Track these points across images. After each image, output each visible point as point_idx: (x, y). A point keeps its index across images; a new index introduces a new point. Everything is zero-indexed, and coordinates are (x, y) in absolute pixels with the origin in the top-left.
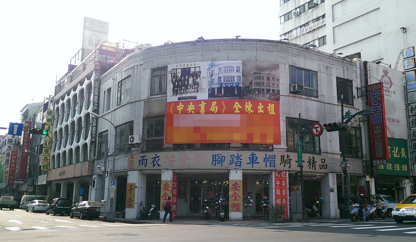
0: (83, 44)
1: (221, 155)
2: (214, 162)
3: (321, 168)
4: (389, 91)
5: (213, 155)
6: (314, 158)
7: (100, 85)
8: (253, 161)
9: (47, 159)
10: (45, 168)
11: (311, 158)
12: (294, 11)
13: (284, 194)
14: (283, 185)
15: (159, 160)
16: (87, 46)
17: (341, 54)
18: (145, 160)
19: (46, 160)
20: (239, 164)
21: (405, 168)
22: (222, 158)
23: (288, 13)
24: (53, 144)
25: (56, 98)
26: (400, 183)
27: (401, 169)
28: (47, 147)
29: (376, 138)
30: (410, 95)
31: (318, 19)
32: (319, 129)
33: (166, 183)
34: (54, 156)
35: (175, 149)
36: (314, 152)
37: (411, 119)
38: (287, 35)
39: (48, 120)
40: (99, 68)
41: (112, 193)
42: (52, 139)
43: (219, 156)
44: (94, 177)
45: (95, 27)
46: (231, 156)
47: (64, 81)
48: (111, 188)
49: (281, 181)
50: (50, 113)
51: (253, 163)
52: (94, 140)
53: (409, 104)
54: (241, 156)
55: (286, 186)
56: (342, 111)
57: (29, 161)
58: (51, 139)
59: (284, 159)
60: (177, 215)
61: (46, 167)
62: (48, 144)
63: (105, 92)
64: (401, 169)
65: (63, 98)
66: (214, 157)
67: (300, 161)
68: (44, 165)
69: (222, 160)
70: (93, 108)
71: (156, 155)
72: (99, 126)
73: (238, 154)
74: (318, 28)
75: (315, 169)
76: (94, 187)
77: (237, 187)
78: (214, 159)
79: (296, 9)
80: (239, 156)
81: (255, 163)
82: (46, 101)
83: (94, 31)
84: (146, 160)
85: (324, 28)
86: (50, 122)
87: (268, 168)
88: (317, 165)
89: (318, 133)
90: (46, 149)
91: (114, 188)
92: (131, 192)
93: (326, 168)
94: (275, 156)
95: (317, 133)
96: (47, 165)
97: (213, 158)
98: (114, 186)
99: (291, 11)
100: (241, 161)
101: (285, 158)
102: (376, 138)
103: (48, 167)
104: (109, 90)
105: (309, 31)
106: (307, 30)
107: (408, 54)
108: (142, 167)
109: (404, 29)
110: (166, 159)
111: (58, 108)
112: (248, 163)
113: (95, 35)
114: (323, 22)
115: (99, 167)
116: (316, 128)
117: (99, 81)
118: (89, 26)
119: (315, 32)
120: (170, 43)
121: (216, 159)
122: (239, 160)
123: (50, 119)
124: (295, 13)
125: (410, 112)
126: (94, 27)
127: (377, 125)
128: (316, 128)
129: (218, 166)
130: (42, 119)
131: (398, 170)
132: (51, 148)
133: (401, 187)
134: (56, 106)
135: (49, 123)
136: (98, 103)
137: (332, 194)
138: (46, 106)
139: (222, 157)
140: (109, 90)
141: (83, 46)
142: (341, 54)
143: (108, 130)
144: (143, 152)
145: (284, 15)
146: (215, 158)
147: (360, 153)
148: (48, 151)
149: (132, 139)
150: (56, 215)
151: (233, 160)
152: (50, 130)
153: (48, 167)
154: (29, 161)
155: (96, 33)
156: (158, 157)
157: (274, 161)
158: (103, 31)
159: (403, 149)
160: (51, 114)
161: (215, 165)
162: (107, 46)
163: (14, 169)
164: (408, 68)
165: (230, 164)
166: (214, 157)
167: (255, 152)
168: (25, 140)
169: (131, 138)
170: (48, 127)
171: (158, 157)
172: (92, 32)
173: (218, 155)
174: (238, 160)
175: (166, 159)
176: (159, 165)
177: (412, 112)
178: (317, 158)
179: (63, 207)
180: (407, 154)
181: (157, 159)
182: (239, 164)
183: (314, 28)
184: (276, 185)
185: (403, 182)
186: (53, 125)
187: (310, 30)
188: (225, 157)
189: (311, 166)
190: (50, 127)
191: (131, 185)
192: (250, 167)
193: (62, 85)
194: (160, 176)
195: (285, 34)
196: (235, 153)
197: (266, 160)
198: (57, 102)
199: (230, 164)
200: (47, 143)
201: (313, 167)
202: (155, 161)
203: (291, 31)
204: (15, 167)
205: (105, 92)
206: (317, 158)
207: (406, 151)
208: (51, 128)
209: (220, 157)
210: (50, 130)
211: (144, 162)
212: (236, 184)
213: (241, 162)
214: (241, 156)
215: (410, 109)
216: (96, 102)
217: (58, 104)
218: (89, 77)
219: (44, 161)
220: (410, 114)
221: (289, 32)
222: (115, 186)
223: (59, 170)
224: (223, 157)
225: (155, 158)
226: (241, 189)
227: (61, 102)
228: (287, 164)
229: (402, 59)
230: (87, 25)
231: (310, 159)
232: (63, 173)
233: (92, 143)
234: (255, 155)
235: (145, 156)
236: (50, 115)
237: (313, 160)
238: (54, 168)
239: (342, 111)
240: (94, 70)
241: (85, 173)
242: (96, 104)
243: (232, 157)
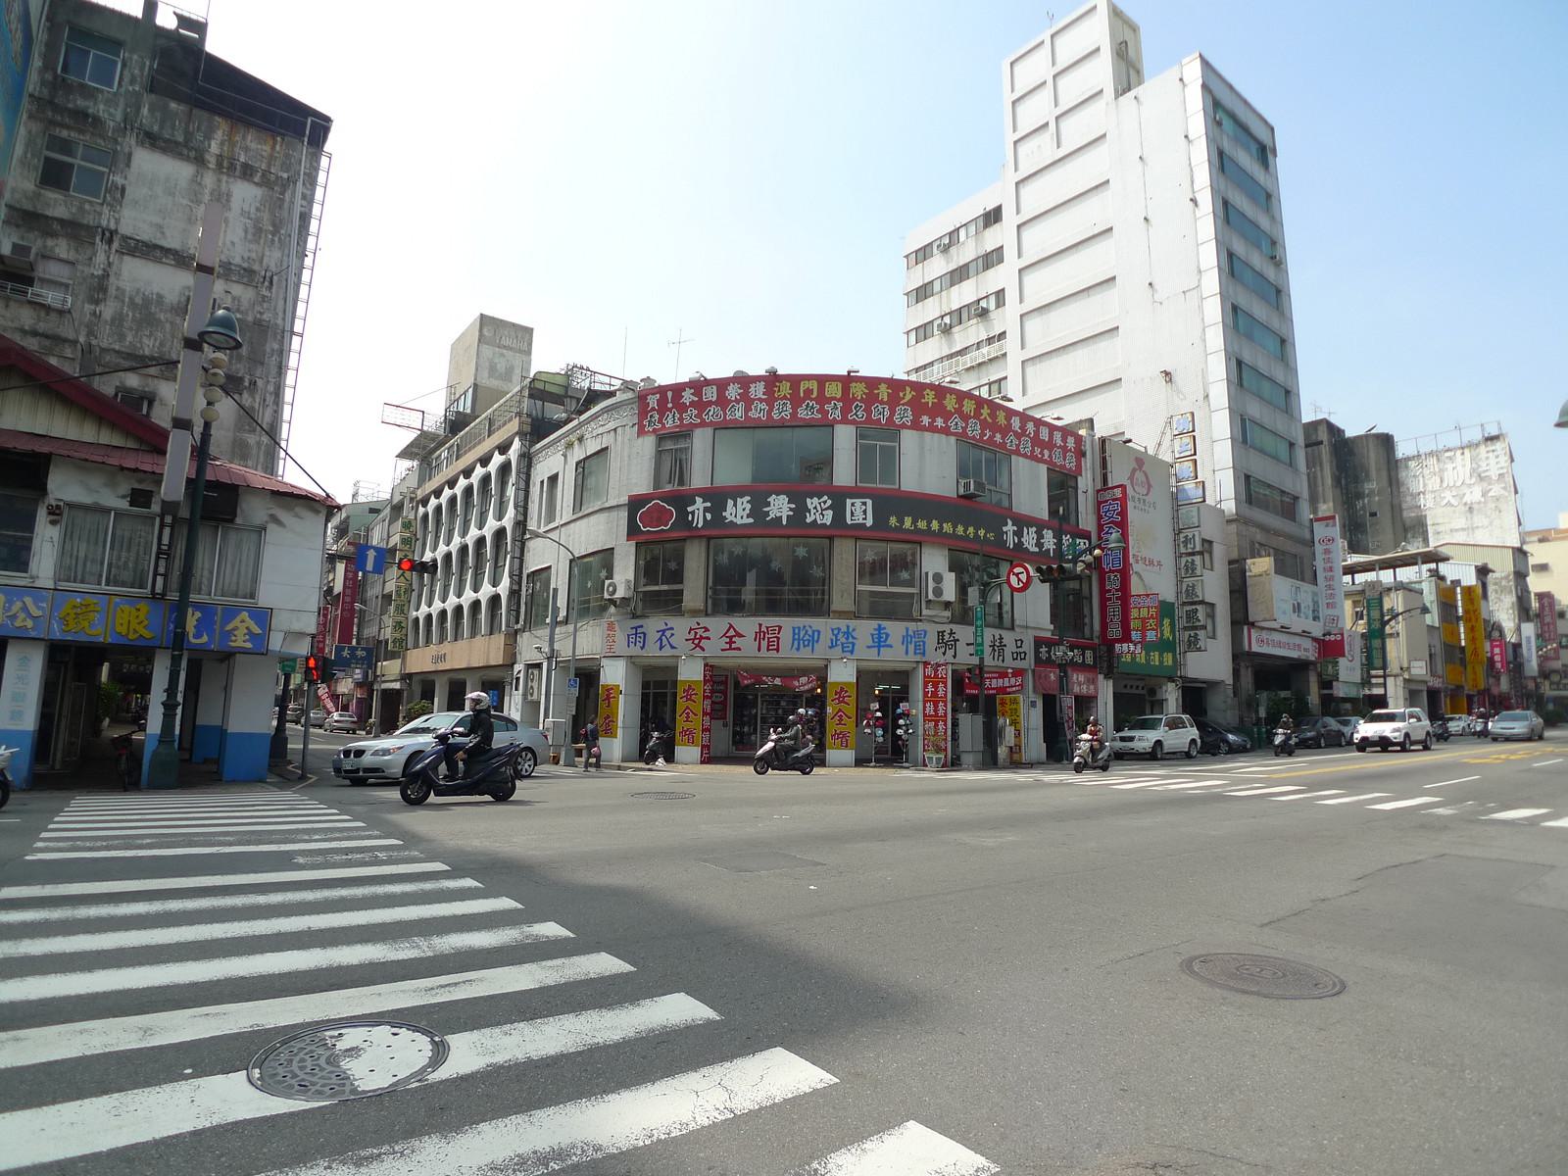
0: (476, 376)
1: (810, 627)
2: (796, 642)
3: (1014, 659)
4: (1144, 501)
5: (939, 632)
6: (1001, 638)
7: (529, 466)
8: (880, 641)
11: (998, 637)
12: (939, 321)
13: (941, 712)
14: (941, 693)
15: (673, 635)
16: (485, 381)
17: (1058, 419)
18: (642, 635)
20: (849, 649)
21: (1168, 659)
22: (813, 634)
23: (925, 325)
24: (415, 595)
25: (420, 494)
26: (1158, 691)
27: (1161, 662)
29: (1110, 599)
30: (1184, 511)
31: (990, 340)
32: (1023, 577)
33: (842, 689)
34: (417, 619)
35: (709, 611)
36: (1000, 625)
37: (1184, 560)
39: (404, 541)
40: (529, 430)
43: (807, 631)
44: (517, 667)
46: (832, 630)
47: (440, 455)
49: (935, 686)
50: (407, 525)
51: (879, 647)
52: (515, 587)
53: (1180, 531)
54: (854, 630)
55: (946, 695)
57: (355, 629)
59: (943, 639)
60: (712, 754)
63: (542, 482)
64: (1161, 662)
65: (438, 493)
66: (797, 631)
67: (977, 645)
69: (813, 638)
70: (516, 515)
71: (666, 625)
72: (528, 557)
73: (848, 627)
74: (990, 360)
75: (1003, 661)
76: (516, 689)
77: (844, 697)
78: (797, 637)
79: (942, 317)
80: (851, 630)
81: (883, 646)
82: (397, 499)
84: (645, 634)
87: (911, 657)
88: (1008, 652)
89: (1021, 585)
92: (609, 702)
93: (1024, 659)
94: (780, 628)
97: (794, 634)
99: (932, 322)
100: (854, 641)
101: (947, 637)
102: (1110, 599)
103: (404, 644)
104: (553, 479)
105: (969, 366)
106: (965, 363)
107: (1181, 428)
108: (635, 650)
109: (1167, 373)
110: (689, 633)
111: (426, 515)
112: (869, 647)
113: (502, 355)
114: (1001, 349)
115: (531, 647)
116: (1017, 575)
117: (527, 460)
119: (984, 368)
120: (702, 379)
121: (801, 636)
122: (851, 640)
124: (939, 325)
125: (1182, 545)
127: (1113, 572)
128: (1017, 575)
129: (805, 652)
130: (385, 536)
131: (1157, 663)
132: (410, 601)
133: (1158, 697)
134: (421, 510)
135: (406, 548)
136: (526, 508)
137: (1033, 711)
138: (397, 509)
139: (814, 632)
140: (553, 479)
141: (475, 379)
142: (1058, 419)
143: (550, 567)
144: (634, 616)
145: (916, 329)
146: (799, 634)
147: (1087, 630)
149: (611, 589)
151: (837, 640)
153: (404, 644)
154: (355, 629)
156: (672, 629)
157: (778, 639)
159: (1166, 622)
161: (798, 649)
163: (321, 645)
164: (1182, 455)
165: (830, 647)
166: (797, 631)
167: (884, 623)
169: (609, 585)
171: (672, 629)
172: (497, 349)
173: (804, 627)
174: (847, 639)
175: (689, 633)
176: (673, 647)
177: (1186, 546)
178: (1009, 638)
179: (179, 710)
180: (1173, 631)
181: (668, 634)
182: (849, 649)
184: (926, 694)
185: (1164, 688)
186: (414, 552)
188: (819, 632)
189: (996, 654)
191: (609, 689)
192: (872, 654)
193: (434, 465)
194: (675, 669)
195: (917, 370)
196: (842, 624)
197: (906, 639)
198: (425, 502)
199: (830, 647)
201: (999, 656)
202: (664, 637)
203: (931, 364)
204: (324, 642)
205: (542, 482)
206: (1009, 638)
207: (1172, 625)
209: (810, 633)
211: (638, 639)
212: (842, 689)
213: (853, 644)
214: (854, 630)
215: (1182, 540)
216: (522, 504)
217: (427, 505)
218: (503, 448)
220: (1183, 550)
221: (925, 365)
223: (433, 649)
224: (816, 634)
225: (664, 631)
226: (852, 700)
227: (433, 502)
228: (804, 646)
229: (1168, 437)
231: (995, 641)
232: (442, 658)
233: (514, 594)
234: (885, 628)
235: (642, 626)
237: (1001, 642)
238: (416, 646)
240: (517, 433)
241: (497, 658)
242: (521, 510)
243: (836, 632)
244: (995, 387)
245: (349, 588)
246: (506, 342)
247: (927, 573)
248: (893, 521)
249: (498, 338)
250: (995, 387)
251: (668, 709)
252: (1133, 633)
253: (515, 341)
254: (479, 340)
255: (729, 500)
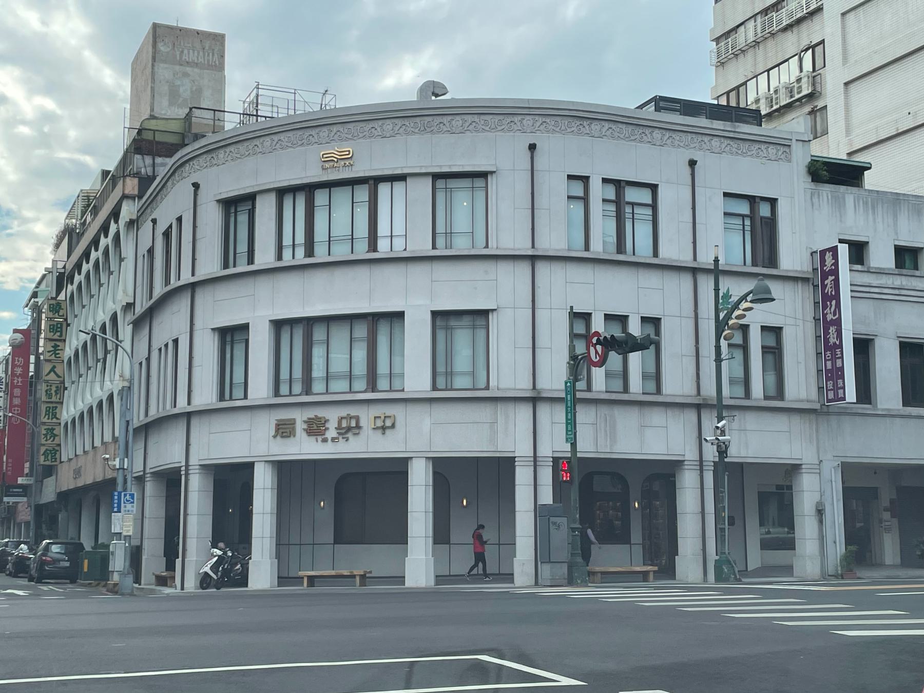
9: (52, 433)
10: (49, 457)
19: (50, 438)
28: (52, 402)
38: (723, 43)
41: (127, 524)
42: (64, 381)
45: (186, 51)
48: (125, 511)
56: (717, 290)
58: (62, 379)
61: (52, 456)
62: (54, 394)
68: (47, 450)
83: (181, 65)
85: (817, 19)
86: (58, 334)
90: (51, 405)
91: (132, 511)
95: (596, 358)
96: (54, 449)
98: (133, 507)
105: (784, 24)
106: (780, 22)
113: (186, 75)
118: (169, 49)
123: (57, 324)
126: (182, 52)
135: (56, 337)
148: (56, 413)
150: (43, 581)
152: (58, 354)
155: (188, 69)
158: (208, 61)
160: (58, 312)
162: (154, 131)
168: (16, 381)
170: (52, 347)
172: (177, 68)
183: (798, 16)
187: (788, 22)
190: (59, 346)
200: (53, 392)
208: (59, 348)
210: (58, 354)
219: (46, 440)
222: (135, 505)
230: (162, 48)
236: (56, 315)
239: (717, 290)
244: (733, 95)
245: (18, 387)
246: (192, 56)
247: (863, 346)
248: (727, 473)
249: (178, 53)
250: (733, 95)
251: (825, 115)
252: (148, 160)
253: (201, 53)
254: (154, 59)
255: (16, 130)
